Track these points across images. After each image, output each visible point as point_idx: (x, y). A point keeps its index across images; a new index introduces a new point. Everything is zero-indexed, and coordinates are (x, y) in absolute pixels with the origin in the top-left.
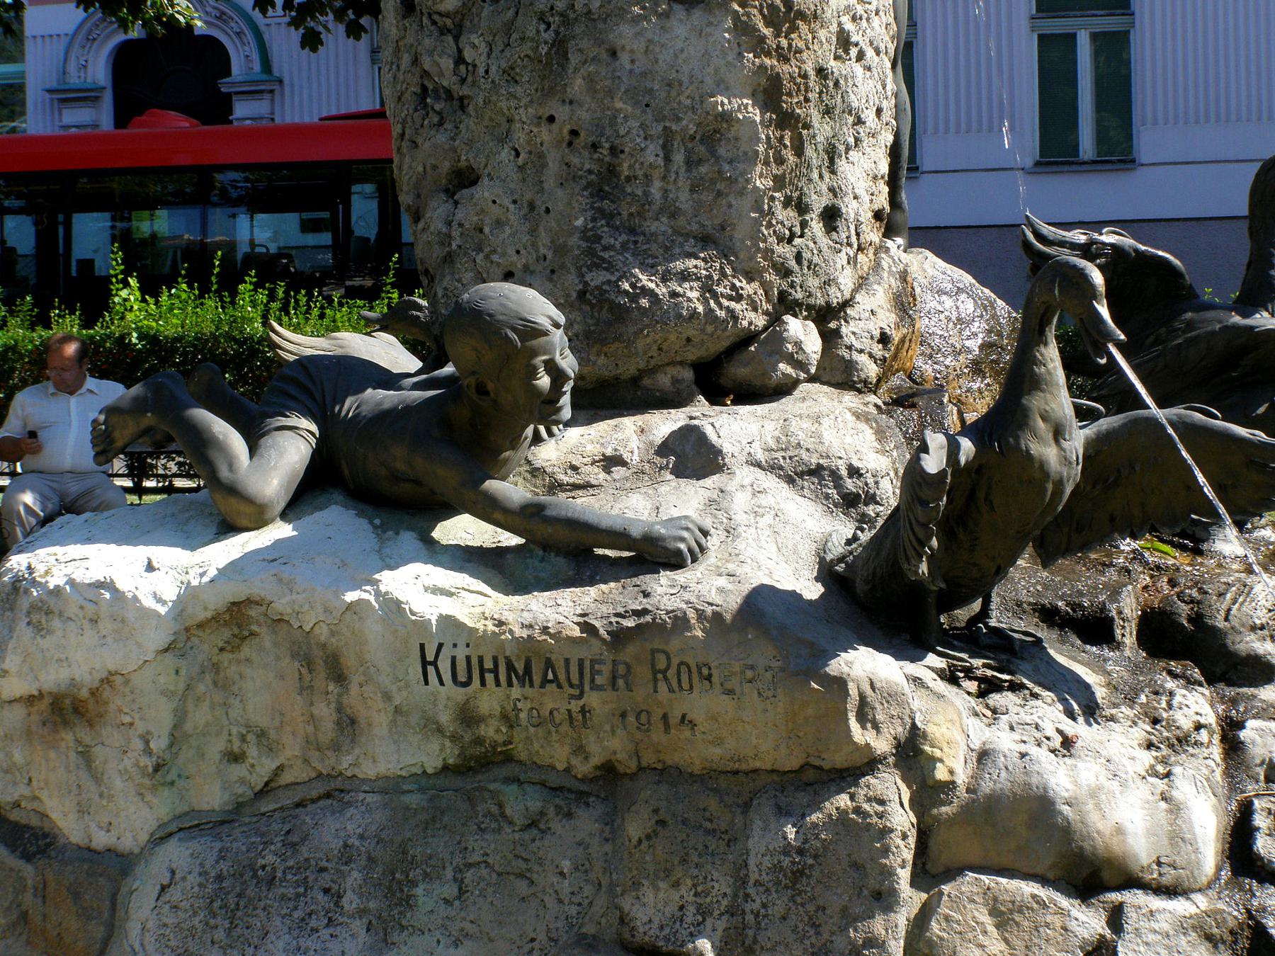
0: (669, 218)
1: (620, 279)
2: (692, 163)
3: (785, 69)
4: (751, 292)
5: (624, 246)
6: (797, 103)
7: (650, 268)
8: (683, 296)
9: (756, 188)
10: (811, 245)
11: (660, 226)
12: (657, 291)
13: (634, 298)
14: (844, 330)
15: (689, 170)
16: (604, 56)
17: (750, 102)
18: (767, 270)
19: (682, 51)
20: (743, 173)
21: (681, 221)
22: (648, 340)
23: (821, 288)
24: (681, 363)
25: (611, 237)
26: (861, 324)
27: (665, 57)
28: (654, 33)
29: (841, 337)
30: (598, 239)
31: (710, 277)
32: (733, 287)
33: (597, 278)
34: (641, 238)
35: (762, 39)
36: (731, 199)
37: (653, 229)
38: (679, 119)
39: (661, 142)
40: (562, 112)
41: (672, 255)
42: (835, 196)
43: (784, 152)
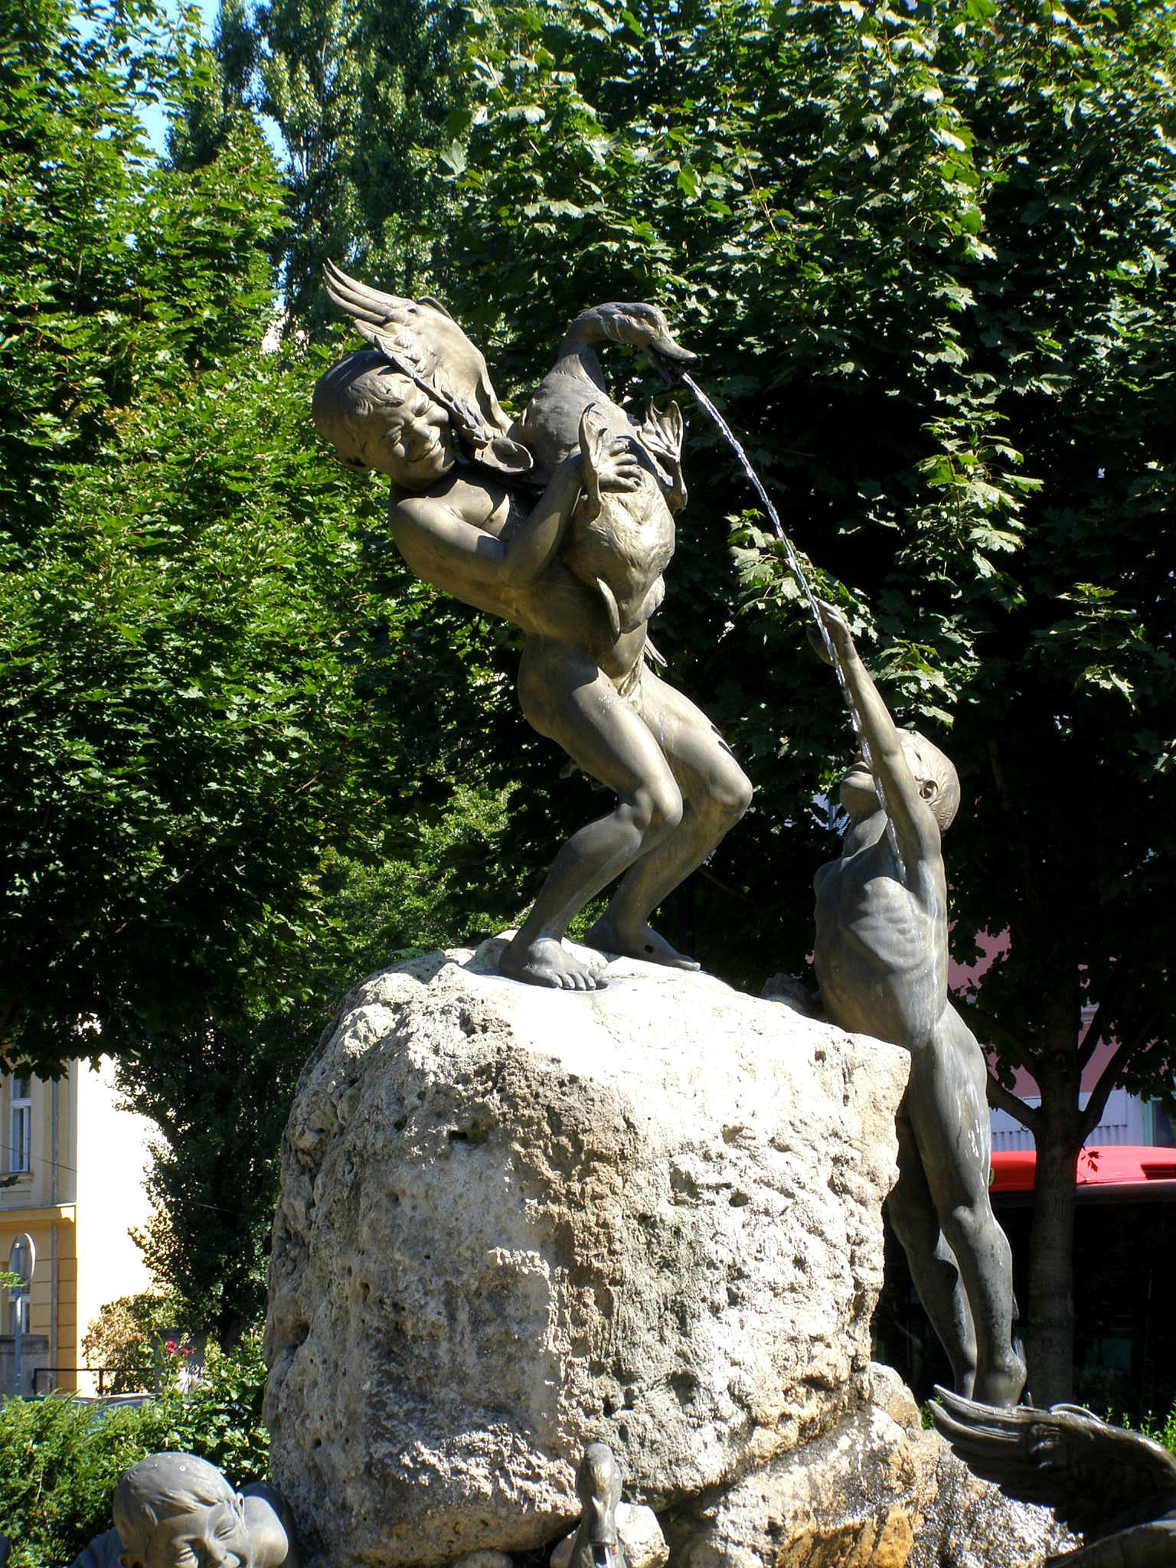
0: (458, 1383)
1: (401, 1452)
2: (477, 1322)
3: (576, 1218)
4: (555, 1471)
5: (409, 1415)
6: (595, 1256)
7: (432, 1442)
8: (466, 1473)
9: (548, 1352)
10: (647, 1418)
11: (448, 1393)
12: (439, 1466)
13: (414, 1474)
14: (721, 1519)
15: (475, 1331)
16: (385, 1202)
17: (537, 1254)
18: (574, 1447)
19: (461, 1196)
20: (533, 1335)
21: (469, 1388)
22: (437, 1522)
23: (664, 1468)
24: (491, 1549)
25: (396, 1403)
26: (744, 1512)
27: (445, 1203)
28: (433, 1176)
29: (716, 1527)
30: (383, 1405)
31: (499, 1453)
32: (529, 1465)
33: (381, 1449)
34: (428, 1407)
35: (548, 1183)
36: (524, 1364)
37: (442, 1395)
38: (459, 1273)
39: (443, 1298)
40: (354, 1261)
41: (459, 1426)
42: (687, 1361)
43: (583, 1311)
